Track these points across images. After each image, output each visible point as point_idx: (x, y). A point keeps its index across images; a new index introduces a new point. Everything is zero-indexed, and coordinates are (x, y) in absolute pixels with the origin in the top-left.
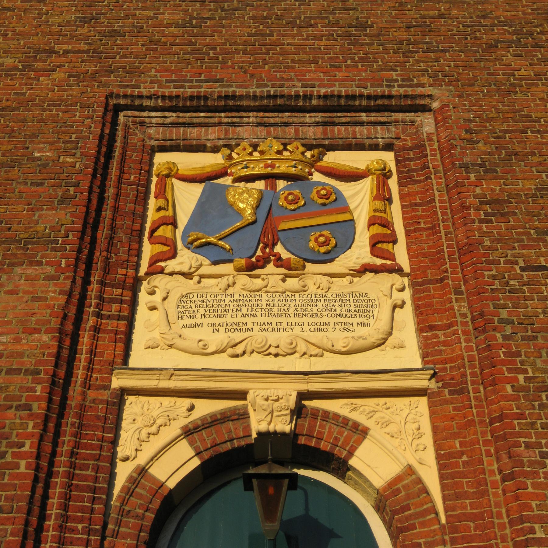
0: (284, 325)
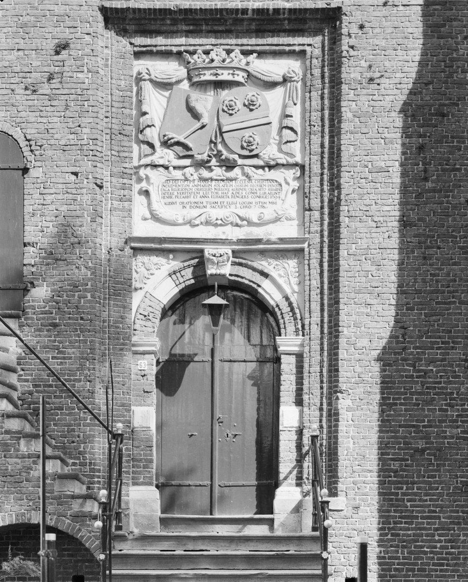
0: (225, 204)
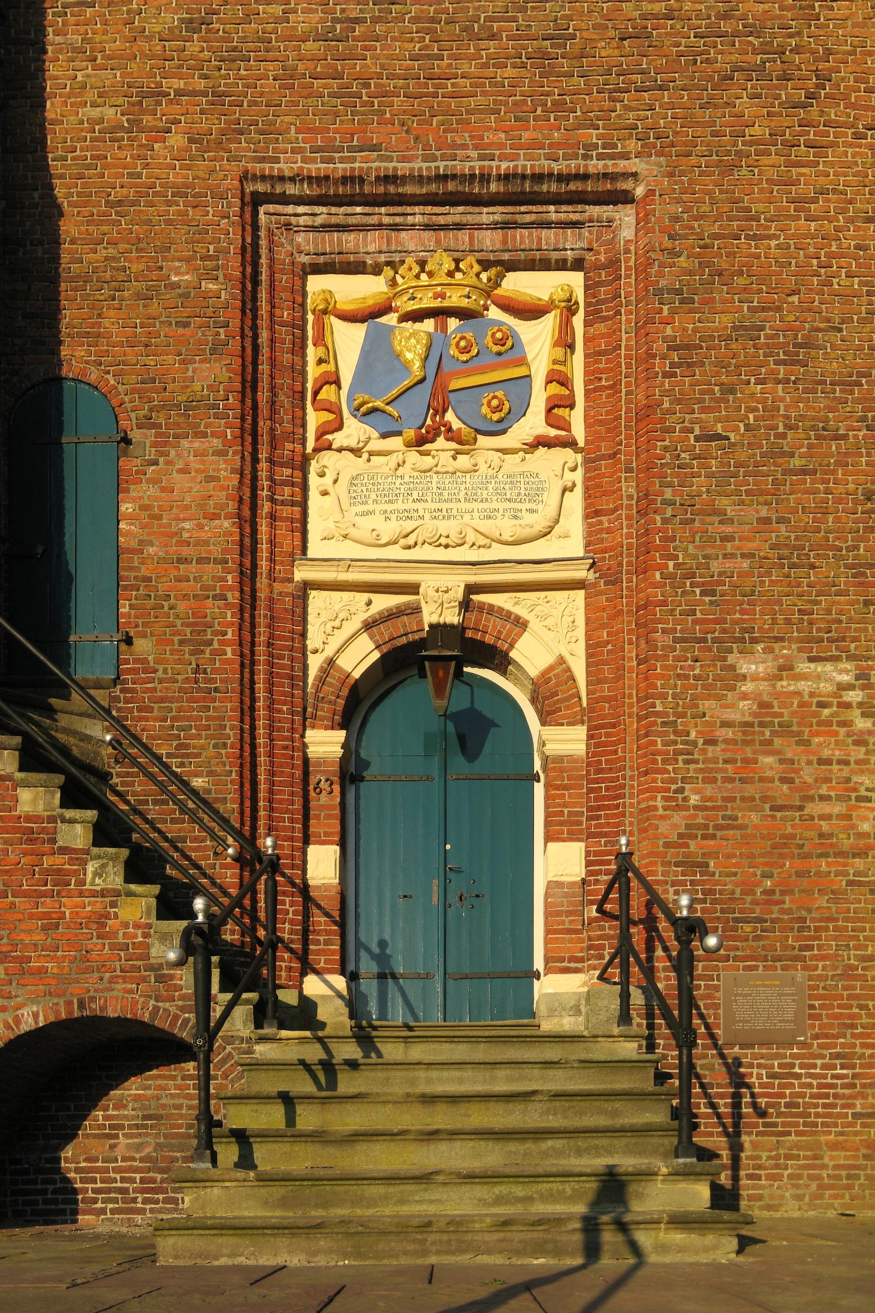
0: (454, 512)
